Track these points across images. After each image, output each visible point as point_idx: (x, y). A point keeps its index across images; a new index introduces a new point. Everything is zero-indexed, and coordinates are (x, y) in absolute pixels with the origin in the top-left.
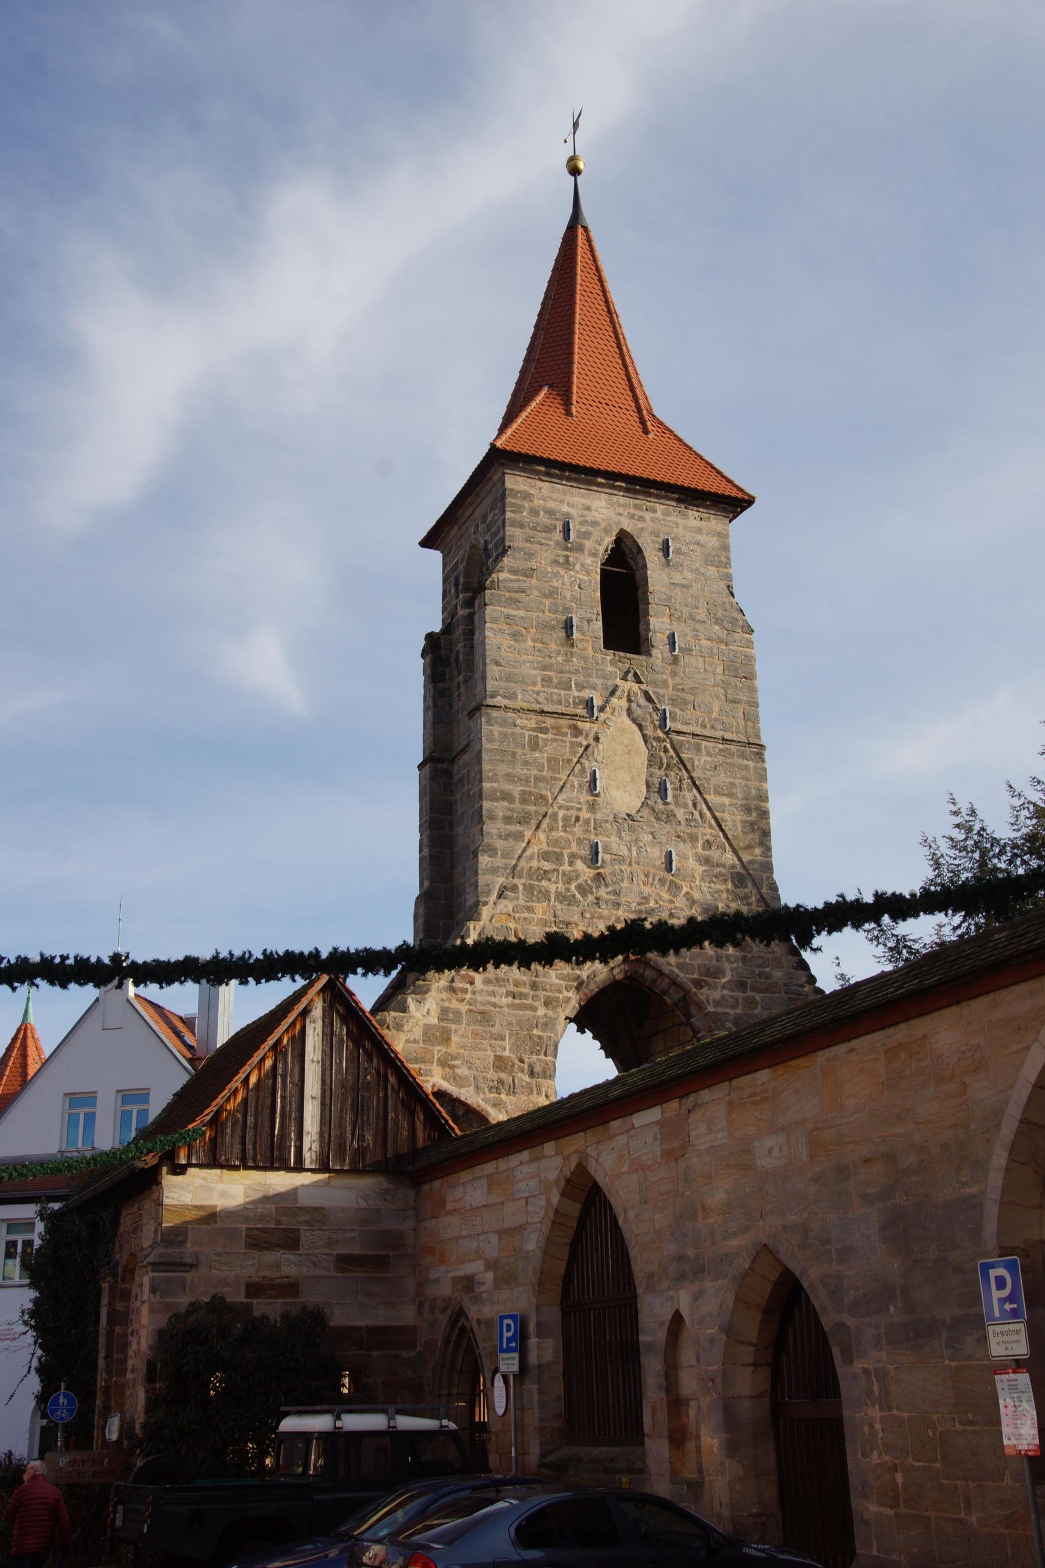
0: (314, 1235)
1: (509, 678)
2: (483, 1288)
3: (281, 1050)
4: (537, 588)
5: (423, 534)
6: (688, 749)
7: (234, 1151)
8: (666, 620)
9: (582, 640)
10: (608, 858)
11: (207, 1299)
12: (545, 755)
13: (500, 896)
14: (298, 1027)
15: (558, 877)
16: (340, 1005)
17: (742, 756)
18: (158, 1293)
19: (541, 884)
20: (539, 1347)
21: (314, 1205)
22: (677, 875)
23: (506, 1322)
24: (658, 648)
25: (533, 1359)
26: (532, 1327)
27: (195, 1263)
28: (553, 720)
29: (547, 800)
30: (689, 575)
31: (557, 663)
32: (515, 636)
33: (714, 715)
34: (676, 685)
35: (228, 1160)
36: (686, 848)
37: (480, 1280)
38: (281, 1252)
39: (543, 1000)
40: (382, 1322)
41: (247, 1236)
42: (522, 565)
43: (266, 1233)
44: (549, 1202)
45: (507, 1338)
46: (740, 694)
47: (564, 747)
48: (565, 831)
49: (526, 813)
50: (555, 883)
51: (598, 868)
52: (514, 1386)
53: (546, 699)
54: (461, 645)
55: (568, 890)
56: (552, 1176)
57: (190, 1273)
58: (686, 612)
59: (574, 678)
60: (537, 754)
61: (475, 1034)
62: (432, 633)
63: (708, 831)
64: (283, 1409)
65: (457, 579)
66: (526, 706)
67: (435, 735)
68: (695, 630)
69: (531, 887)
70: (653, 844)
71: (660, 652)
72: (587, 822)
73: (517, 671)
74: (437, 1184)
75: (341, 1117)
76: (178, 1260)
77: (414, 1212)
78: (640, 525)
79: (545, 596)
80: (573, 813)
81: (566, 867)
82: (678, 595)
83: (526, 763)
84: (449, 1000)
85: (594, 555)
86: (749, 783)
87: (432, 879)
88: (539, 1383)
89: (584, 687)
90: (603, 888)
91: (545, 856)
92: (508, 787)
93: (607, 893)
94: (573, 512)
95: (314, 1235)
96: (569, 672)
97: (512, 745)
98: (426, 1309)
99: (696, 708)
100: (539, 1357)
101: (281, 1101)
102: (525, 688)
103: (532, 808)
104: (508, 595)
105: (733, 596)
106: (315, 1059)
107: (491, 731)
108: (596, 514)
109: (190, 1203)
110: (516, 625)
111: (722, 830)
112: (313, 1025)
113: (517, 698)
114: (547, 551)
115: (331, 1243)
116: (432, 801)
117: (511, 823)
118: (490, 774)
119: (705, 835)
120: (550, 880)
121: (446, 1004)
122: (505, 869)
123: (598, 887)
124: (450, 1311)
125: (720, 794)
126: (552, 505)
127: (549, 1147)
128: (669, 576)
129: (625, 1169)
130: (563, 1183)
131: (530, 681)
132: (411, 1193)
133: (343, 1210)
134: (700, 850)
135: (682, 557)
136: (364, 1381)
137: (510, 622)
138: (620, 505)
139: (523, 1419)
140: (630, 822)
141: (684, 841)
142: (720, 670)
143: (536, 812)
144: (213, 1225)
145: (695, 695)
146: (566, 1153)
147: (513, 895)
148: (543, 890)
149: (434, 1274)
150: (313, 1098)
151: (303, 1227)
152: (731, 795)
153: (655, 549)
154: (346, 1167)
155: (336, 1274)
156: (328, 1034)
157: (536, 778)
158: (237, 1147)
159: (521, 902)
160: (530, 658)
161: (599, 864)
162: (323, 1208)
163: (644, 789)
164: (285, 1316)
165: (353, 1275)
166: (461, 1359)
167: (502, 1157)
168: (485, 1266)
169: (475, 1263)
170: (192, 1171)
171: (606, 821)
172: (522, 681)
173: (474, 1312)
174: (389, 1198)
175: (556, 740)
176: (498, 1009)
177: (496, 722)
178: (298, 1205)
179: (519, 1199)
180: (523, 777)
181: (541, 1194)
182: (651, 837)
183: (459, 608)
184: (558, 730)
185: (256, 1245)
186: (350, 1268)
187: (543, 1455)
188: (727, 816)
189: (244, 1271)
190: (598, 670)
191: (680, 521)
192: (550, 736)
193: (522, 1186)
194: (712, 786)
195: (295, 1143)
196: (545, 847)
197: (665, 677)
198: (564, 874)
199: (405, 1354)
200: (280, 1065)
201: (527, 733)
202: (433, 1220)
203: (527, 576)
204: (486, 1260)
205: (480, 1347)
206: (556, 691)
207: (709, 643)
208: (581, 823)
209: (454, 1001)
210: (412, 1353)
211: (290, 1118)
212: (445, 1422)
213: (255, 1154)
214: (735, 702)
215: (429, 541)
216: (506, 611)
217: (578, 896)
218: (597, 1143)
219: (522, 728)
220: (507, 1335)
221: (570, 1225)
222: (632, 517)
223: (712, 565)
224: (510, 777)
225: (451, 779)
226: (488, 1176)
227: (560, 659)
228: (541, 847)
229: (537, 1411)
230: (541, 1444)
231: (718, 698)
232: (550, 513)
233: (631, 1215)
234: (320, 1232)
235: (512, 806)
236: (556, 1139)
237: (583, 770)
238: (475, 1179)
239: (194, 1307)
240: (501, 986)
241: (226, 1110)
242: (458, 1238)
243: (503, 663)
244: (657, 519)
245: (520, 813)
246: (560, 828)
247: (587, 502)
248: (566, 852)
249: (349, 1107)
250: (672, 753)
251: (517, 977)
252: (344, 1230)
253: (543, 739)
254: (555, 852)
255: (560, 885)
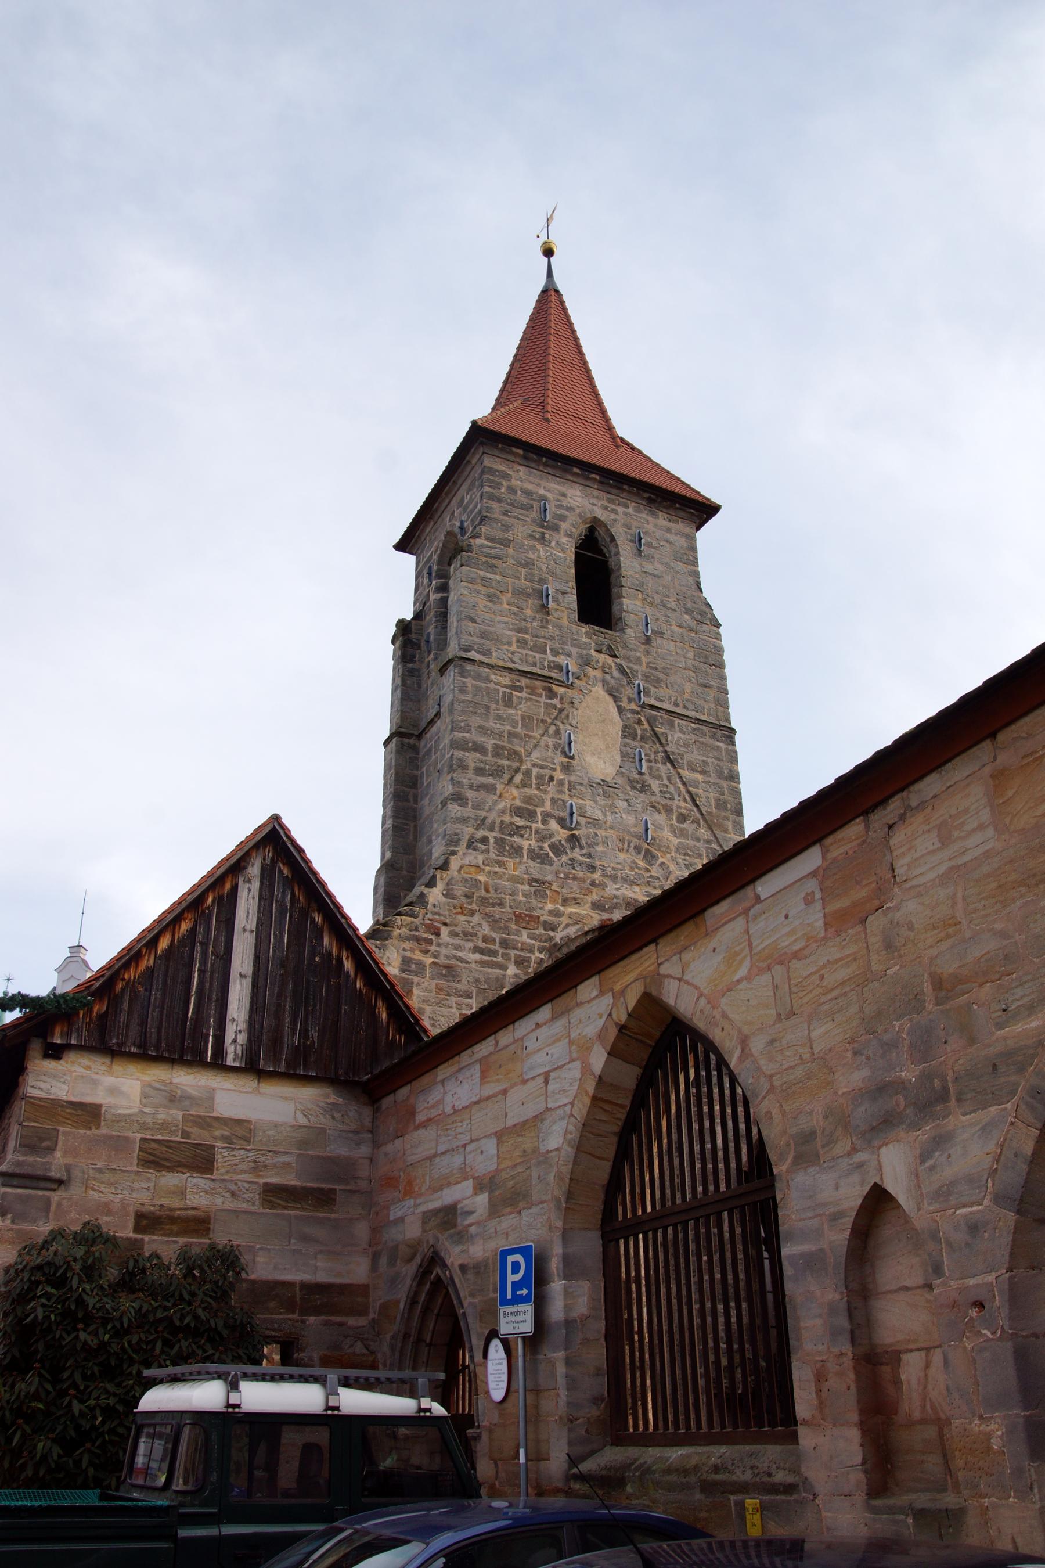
0: (234, 1155)
1: (484, 635)
2: (470, 1220)
3: (203, 912)
4: (513, 557)
5: (397, 536)
6: (662, 724)
7: (130, 1034)
8: (639, 603)
9: (557, 610)
10: (582, 820)
11: (77, 1228)
12: (519, 712)
13: (469, 846)
14: (228, 886)
15: (530, 835)
16: (284, 864)
17: (714, 737)
18: (9, 1216)
19: (513, 839)
20: (567, 1293)
21: (236, 1117)
22: (653, 844)
23: (511, 1259)
24: (631, 627)
25: (556, 1311)
26: (554, 1265)
27: (65, 1178)
28: (528, 681)
29: (520, 756)
30: (660, 567)
31: (533, 628)
32: (491, 597)
33: (686, 696)
34: (649, 663)
35: (120, 1045)
36: (661, 818)
37: (466, 1209)
38: (188, 1174)
39: (513, 959)
40: (322, 1278)
41: (140, 1149)
42: (499, 534)
43: (169, 1147)
44: (586, 1069)
45: (513, 1283)
46: (711, 679)
47: (539, 705)
48: (538, 789)
49: (499, 766)
50: (528, 839)
51: (572, 829)
52: (524, 1355)
53: (520, 659)
54: (432, 627)
55: (541, 848)
56: (592, 1029)
57: (59, 1193)
58: (657, 599)
59: (549, 643)
60: (511, 711)
61: (439, 989)
62: (403, 619)
63: (682, 805)
64: (146, 1373)
65: (430, 568)
66: (500, 663)
67: (402, 712)
68: (666, 616)
69: (503, 840)
70: (628, 813)
71: (632, 634)
72: (561, 783)
73: (492, 629)
74: (403, 1092)
75: (279, 1005)
76: (40, 1173)
77: (370, 1135)
78: (613, 516)
79: (520, 564)
80: (547, 773)
81: (540, 825)
82: (650, 582)
83: (499, 718)
84: (412, 950)
85: (570, 536)
86: (721, 764)
87: (394, 849)
88: (566, 1349)
89: (559, 653)
90: (577, 850)
91: (518, 812)
92: (481, 739)
93: (581, 855)
94: (549, 495)
95: (234, 1155)
96: (544, 637)
97: (486, 699)
98: (383, 1261)
99: (670, 687)
100: (567, 1308)
101: (199, 975)
102: (500, 647)
103: (505, 763)
104: (484, 559)
105: (701, 591)
106: (248, 927)
107: (464, 683)
108: (572, 501)
109: (65, 1098)
110: (492, 588)
111: (697, 806)
112: (247, 885)
113: (491, 655)
114: (524, 526)
115: (256, 1168)
116: (397, 774)
117: (483, 775)
118: (462, 724)
119: (680, 807)
120: (522, 836)
121: (409, 954)
122: (476, 820)
123: (573, 848)
124: (418, 1260)
125: (694, 770)
126: (530, 487)
127: (588, 989)
128: (641, 565)
129: (743, 972)
130: (613, 1033)
131: (505, 640)
132: (367, 1111)
133: (276, 1126)
134: (674, 822)
135: (653, 550)
136: (296, 1355)
137: (487, 584)
138: (594, 497)
139: (537, 1407)
140: (605, 788)
141: (659, 811)
142: (691, 655)
143: (509, 767)
144: (94, 1131)
145: (667, 675)
146: (618, 987)
147: (484, 847)
148: (515, 845)
149: (395, 1213)
150: (242, 976)
151: (220, 1144)
152: (703, 772)
153: (627, 540)
154: (282, 1070)
155: (262, 1210)
156: (265, 899)
157: (509, 733)
158: (134, 1029)
159: (492, 855)
160: (506, 619)
161: (573, 826)
162: (249, 1122)
163: (618, 758)
164: (184, 1257)
165: (286, 1212)
166: (431, 1328)
167: (505, 1026)
168: (474, 1188)
169: (459, 1186)
170: (71, 1056)
171: (581, 784)
172: (497, 640)
173: (454, 1255)
174: (337, 1115)
175: (531, 699)
176: (464, 965)
177: (470, 675)
178: (214, 1114)
179: (533, 1078)
180: (497, 731)
181: (572, 1060)
182: (626, 804)
183: (431, 594)
184: (533, 691)
185: (152, 1162)
186: (281, 1202)
187: (573, 1461)
188: (700, 792)
189: (134, 1195)
190: (572, 639)
191: (650, 519)
192: (524, 695)
193: (540, 1058)
194: (685, 762)
195: (214, 1031)
196: (518, 803)
197: (638, 654)
198: (537, 832)
199: (352, 1321)
200: (201, 930)
201: (501, 689)
202: (396, 1141)
203: (502, 544)
204: (474, 1178)
205: (465, 1305)
206: (530, 653)
207: (680, 630)
208: (555, 783)
209: (417, 952)
210: (362, 1321)
211: (210, 999)
212: (426, 1403)
213: (159, 1041)
214: (706, 687)
215: (402, 546)
216: (482, 573)
217: (551, 855)
218: (680, 953)
219: (496, 684)
220: (511, 1278)
221: (619, 1102)
222: (606, 508)
223: (681, 562)
224: (482, 729)
225: (418, 753)
226: (480, 1061)
227: (535, 624)
228: (513, 802)
229: (563, 1393)
230: (570, 1443)
231: (690, 681)
232: (527, 493)
233: (757, 1045)
234: (242, 1152)
235: (484, 758)
236: (599, 973)
237: (558, 732)
238: (460, 1070)
239: (57, 1235)
240: (468, 940)
241: (123, 979)
242: (431, 1158)
243: (478, 620)
244: (629, 514)
245: (492, 766)
246: (534, 786)
247: (563, 489)
248: (539, 810)
249: (289, 993)
250: (646, 726)
251: (486, 932)
252: (276, 1153)
253: (518, 697)
254: (528, 809)
255: (533, 842)
